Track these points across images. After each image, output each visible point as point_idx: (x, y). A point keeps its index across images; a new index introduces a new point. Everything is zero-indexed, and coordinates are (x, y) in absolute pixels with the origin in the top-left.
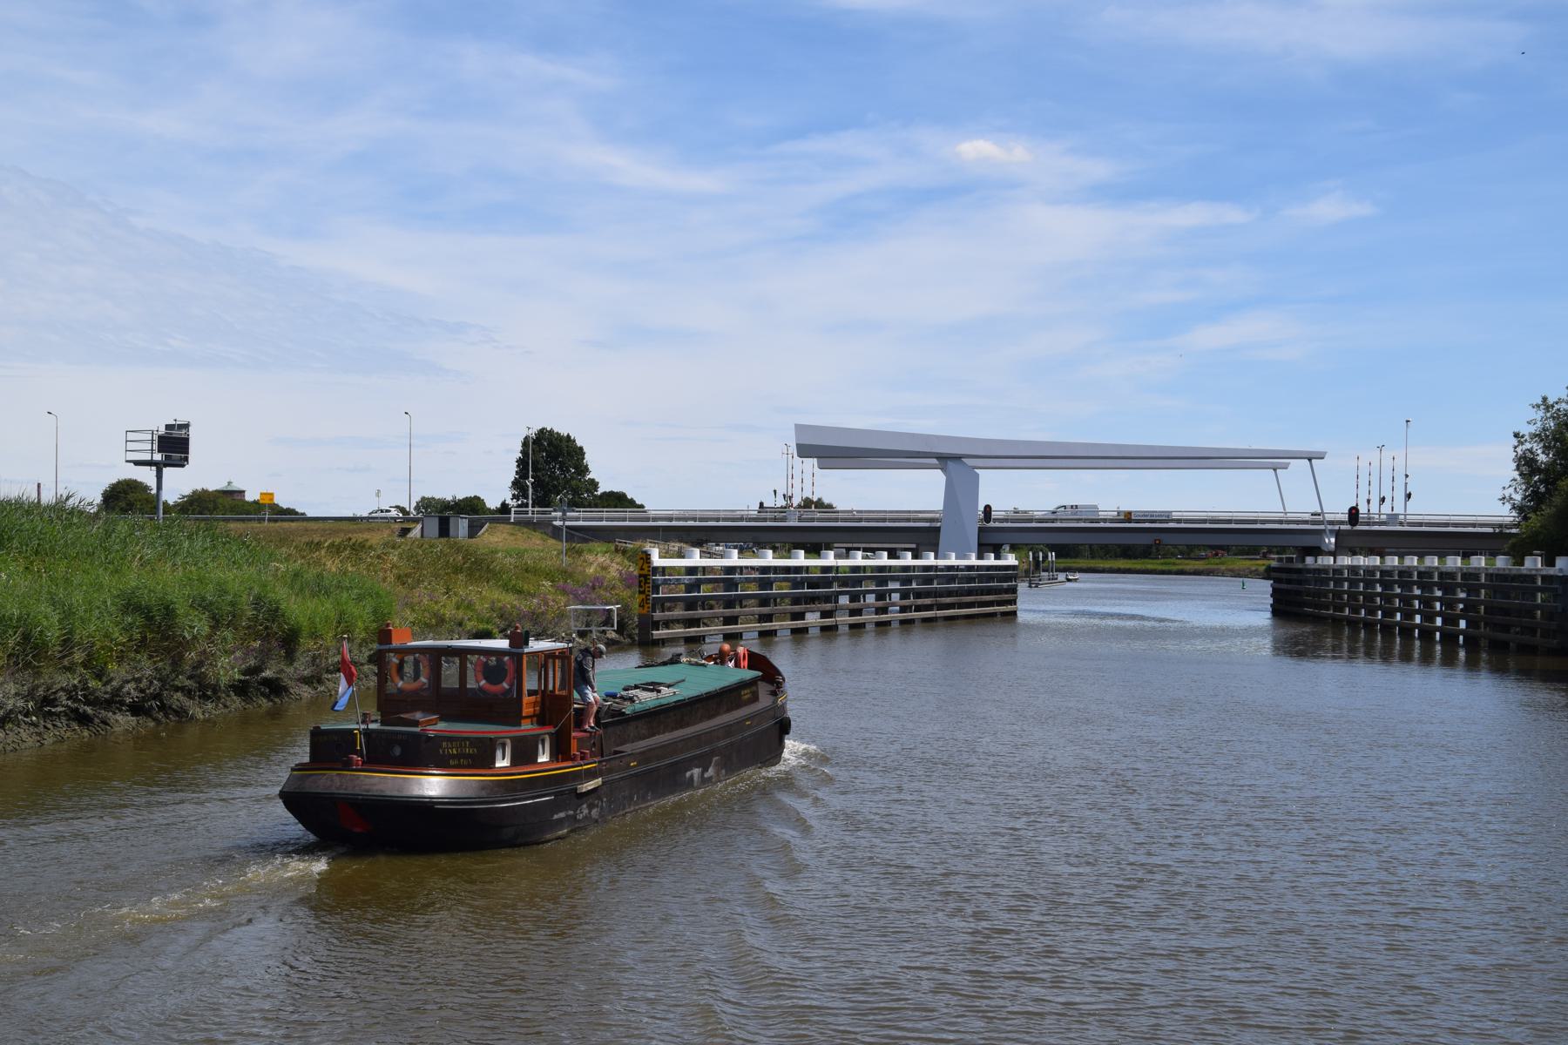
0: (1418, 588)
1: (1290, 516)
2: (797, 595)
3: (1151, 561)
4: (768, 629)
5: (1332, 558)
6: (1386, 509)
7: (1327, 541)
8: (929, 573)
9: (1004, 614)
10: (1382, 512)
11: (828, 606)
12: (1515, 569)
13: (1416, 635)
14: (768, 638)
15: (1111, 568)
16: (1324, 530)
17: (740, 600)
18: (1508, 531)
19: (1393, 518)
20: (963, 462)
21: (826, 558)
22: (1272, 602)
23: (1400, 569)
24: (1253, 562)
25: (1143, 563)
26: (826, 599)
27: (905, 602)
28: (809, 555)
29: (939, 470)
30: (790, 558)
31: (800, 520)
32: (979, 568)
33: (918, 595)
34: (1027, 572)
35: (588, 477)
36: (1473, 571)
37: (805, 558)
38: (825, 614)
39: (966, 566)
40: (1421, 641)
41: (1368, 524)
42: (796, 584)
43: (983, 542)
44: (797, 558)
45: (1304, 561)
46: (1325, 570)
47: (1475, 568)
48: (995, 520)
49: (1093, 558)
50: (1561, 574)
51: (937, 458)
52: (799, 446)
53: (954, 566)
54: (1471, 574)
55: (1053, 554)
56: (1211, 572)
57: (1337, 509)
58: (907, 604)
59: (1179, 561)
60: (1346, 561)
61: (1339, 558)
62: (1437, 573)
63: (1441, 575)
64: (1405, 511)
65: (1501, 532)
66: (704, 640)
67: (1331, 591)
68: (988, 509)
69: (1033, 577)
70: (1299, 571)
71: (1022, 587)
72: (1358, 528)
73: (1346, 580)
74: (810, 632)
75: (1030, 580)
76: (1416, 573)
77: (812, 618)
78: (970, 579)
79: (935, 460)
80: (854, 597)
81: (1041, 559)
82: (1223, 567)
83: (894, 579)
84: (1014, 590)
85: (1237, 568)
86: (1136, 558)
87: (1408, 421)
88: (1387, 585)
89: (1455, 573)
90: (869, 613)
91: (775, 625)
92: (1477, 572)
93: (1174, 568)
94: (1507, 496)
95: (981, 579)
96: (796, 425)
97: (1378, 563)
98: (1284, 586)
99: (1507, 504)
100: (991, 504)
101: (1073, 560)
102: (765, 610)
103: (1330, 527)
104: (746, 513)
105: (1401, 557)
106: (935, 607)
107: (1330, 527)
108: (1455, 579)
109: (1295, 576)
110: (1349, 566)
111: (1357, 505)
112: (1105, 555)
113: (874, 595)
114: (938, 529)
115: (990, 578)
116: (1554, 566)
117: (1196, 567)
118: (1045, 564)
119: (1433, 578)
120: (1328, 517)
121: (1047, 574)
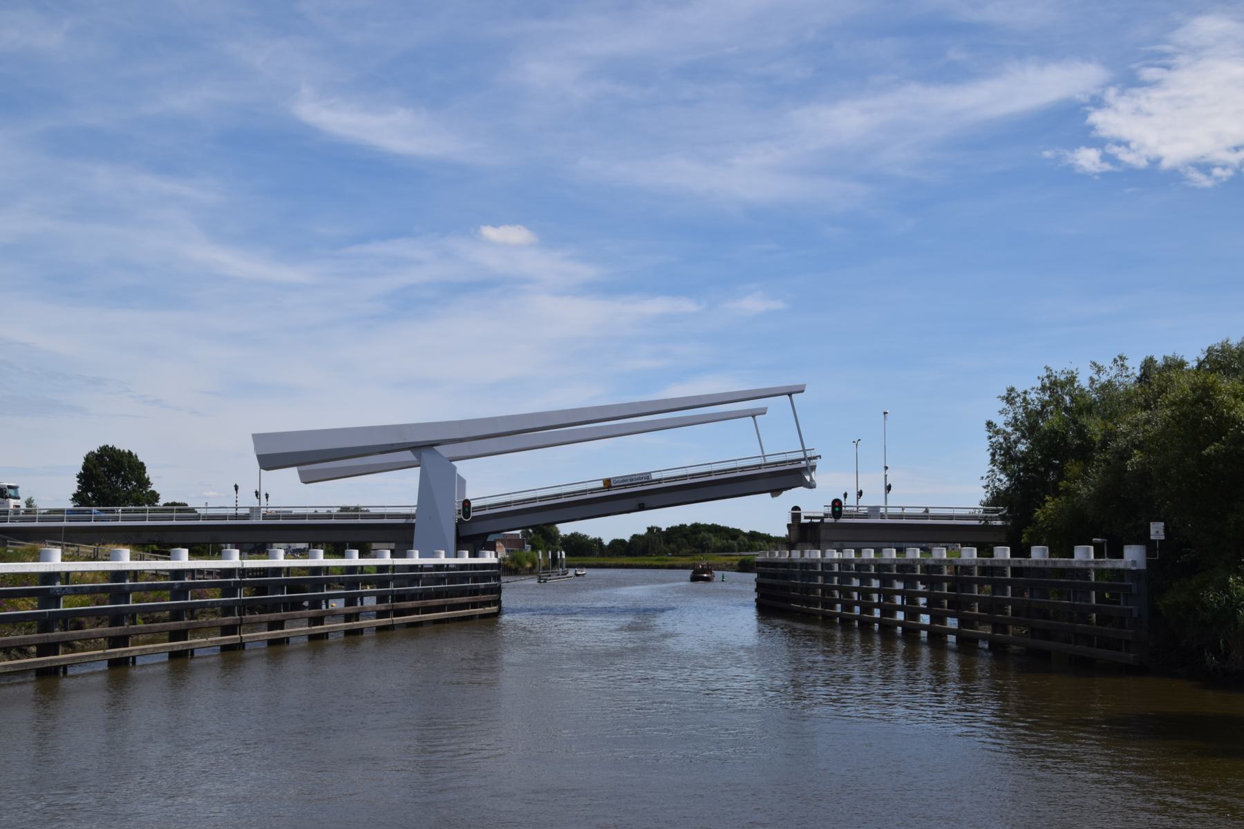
4: (118, 656)
5: (819, 552)
12: (1061, 562)
15: (616, 564)
19: (874, 510)
20: (434, 449)
22: (756, 597)
23: (858, 562)
24: (728, 558)
25: (641, 560)
27: (382, 607)
28: (328, 556)
30: (405, 557)
33: (400, 597)
35: (150, 489)
37: (324, 558)
39: (457, 565)
41: (851, 517)
46: (813, 564)
50: (1134, 568)
53: (417, 565)
59: (669, 558)
61: (794, 552)
62: (1009, 568)
66: (65, 672)
67: (819, 586)
72: (842, 520)
73: (836, 574)
76: (919, 567)
78: (439, 580)
79: (409, 452)
80: (350, 601)
83: (367, 582)
85: (716, 563)
86: (636, 556)
87: (885, 413)
88: (886, 581)
89: (973, 566)
90: (368, 617)
91: (131, 651)
93: (667, 563)
95: (452, 579)
98: (769, 581)
108: (972, 574)
110: (839, 559)
114: (413, 526)
115: (464, 578)
116: (1122, 557)
117: (684, 562)
119: (915, 572)
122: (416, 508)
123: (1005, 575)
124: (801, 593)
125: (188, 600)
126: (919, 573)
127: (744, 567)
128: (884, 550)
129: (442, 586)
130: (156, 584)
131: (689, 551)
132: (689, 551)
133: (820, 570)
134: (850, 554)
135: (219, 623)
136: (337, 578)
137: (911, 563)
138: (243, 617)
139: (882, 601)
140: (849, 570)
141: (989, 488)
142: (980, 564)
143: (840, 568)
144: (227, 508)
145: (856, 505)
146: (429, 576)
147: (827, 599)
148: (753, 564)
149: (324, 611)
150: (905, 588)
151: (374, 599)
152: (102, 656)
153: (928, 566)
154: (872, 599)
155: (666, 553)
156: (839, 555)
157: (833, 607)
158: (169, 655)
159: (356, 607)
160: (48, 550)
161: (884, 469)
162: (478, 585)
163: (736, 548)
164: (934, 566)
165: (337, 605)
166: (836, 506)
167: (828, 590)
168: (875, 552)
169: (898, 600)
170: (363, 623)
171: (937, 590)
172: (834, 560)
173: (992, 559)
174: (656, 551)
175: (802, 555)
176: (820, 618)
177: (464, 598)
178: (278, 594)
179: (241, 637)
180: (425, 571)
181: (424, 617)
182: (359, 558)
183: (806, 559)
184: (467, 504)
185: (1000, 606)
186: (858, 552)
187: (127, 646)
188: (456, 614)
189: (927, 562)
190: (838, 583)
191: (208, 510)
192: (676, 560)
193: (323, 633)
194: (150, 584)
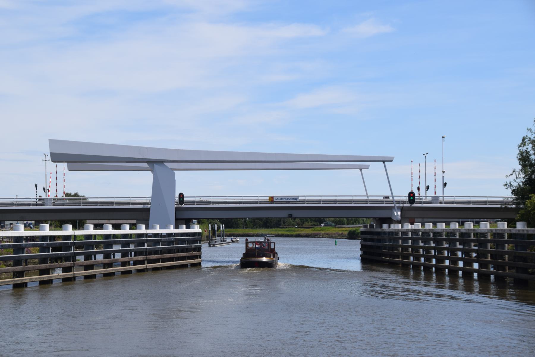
0: (434, 243)
1: (371, 199)
2: (43, 257)
3: (280, 229)
5: (400, 225)
6: (431, 193)
7: (396, 214)
8: (141, 239)
9: (193, 265)
10: (427, 195)
11: (68, 264)
13: (447, 274)
14: (20, 289)
16: (394, 207)
17: (26, 260)
18: (510, 207)
19: (436, 199)
20: (164, 164)
21: (66, 229)
22: (361, 254)
24: (340, 229)
26: (67, 258)
29: (150, 172)
30: (136, 229)
31: (54, 204)
32: (176, 235)
34: (208, 237)
36: (500, 232)
37: (50, 230)
38: (66, 270)
40: (450, 277)
42: (43, 249)
43: (177, 218)
44: (43, 230)
45: (381, 227)
46: (396, 232)
47: (502, 230)
48: (187, 203)
49: (246, 228)
51: (147, 162)
52: (52, 154)
53: (159, 234)
54: (498, 234)
55: (224, 225)
56: (315, 235)
57: (402, 194)
58: (126, 260)
59: (296, 229)
60: (408, 226)
63: (476, 234)
64: (426, 195)
65: (506, 207)
67: (400, 246)
68: (181, 196)
69: (211, 240)
70: (378, 233)
71: (205, 247)
72: (415, 205)
73: (410, 238)
74: (53, 283)
75: (210, 242)
76: (458, 234)
77: (58, 273)
78: (170, 242)
79: (146, 164)
80: (88, 257)
81: (216, 229)
82: (323, 232)
83: (116, 243)
84: (199, 249)
86: (272, 227)
87: (443, 137)
88: (438, 242)
89: (486, 233)
91: (25, 279)
92: (503, 232)
93: (295, 233)
94: (508, 183)
95: (177, 242)
96: (50, 141)
97: (420, 227)
98: (369, 243)
99: (509, 188)
100: (182, 193)
101: (234, 230)
102: (18, 268)
103: (397, 205)
104: (15, 200)
105: (477, 223)
106: (146, 262)
107: (397, 205)
109: (376, 237)
111: (412, 190)
112: (254, 226)
113: (120, 254)
114: (149, 209)
115: (183, 241)
117: (307, 233)
118: (219, 232)
120: (396, 199)
121: (220, 238)
122: (151, 198)
123: (504, 238)
124: (389, 250)
125: (49, 252)
126: (458, 237)
127: (352, 236)
128: (438, 224)
129: (172, 246)
130: (36, 244)
131: (310, 224)
132: (310, 224)
133: (400, 236)
134: (429, 226)
135: (64, 265)
136: (119, 241)
137: (453, 231)
138: (75, 262)
139: (436, 254)
140: (418, 236)
141: (507, 186)
142: (509, 232)
143: (412, 235)
144: (30, 198)
145: (425, 195)
146: (165, 240)
147: (404, 253)
148: (358, 233)
149: (112, 260)
150: (449, 246)
151: (102, 255)
152: (13, 282)
153: (462, 233)
154: (431, 253)
155: (293, 226)
156: (412, 227)
157: (408, 259)
158: (13, 286)
159: (111, 259)
160: (44, 225)
161: (442, 172)
162: (191, 246)
163: (345, 222)
164: (465, 233)
165: (100, 258)
166: (411, 196)
167: (405, 248)
168: (445, 225)
169: (446, 253)
170: (96, 271)
171: (467, 247)
172: (409, 229)
173: (516, 229)
174: (287, 224)
175: (389, 227)
176: (401, 266)
177: (184, 253)
178: (90, 250)
179: (74, 274)
180: (163, 237)
181: (163, 264)
182: (186, 229)
183: (392, 229)
184: (181, 196)
185: (501, 255)
186: (423, 225)
187: (24, 277)
188: (179, 263)
189: (461, 231)
190: (411, 244)
191: (18, 200)
192: (302, 231)
193: (112, 273)
194: (33, 244)
